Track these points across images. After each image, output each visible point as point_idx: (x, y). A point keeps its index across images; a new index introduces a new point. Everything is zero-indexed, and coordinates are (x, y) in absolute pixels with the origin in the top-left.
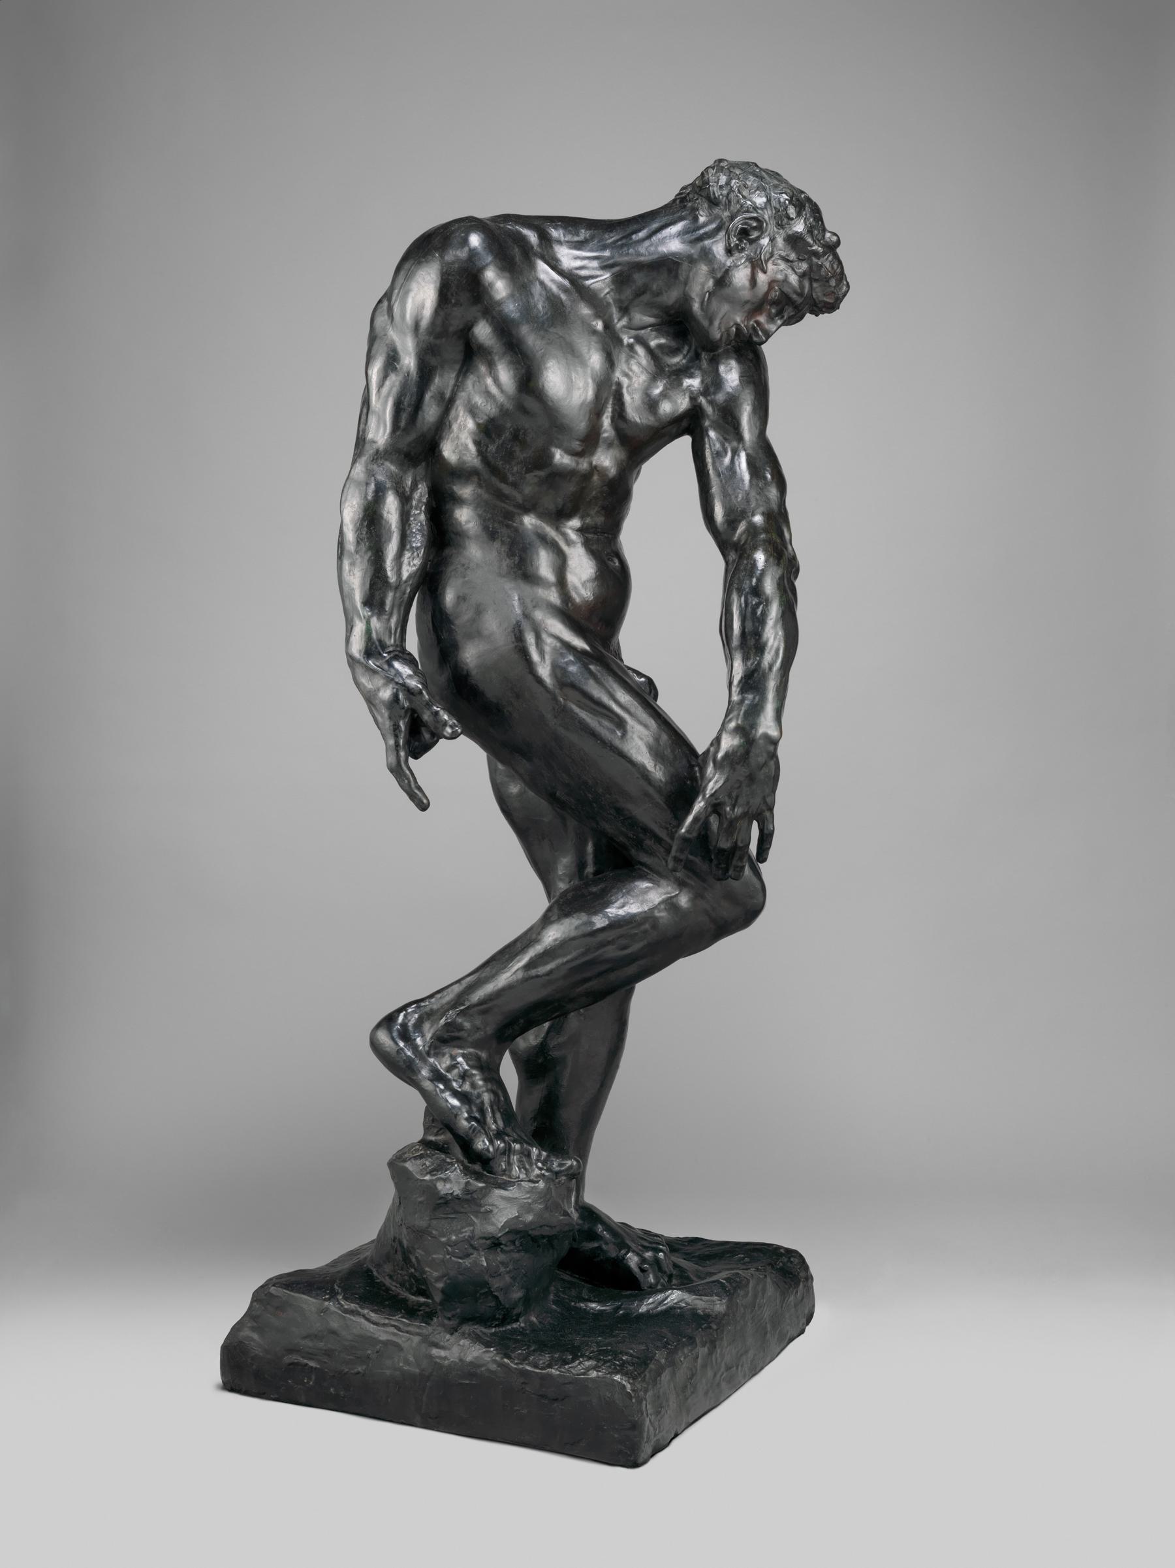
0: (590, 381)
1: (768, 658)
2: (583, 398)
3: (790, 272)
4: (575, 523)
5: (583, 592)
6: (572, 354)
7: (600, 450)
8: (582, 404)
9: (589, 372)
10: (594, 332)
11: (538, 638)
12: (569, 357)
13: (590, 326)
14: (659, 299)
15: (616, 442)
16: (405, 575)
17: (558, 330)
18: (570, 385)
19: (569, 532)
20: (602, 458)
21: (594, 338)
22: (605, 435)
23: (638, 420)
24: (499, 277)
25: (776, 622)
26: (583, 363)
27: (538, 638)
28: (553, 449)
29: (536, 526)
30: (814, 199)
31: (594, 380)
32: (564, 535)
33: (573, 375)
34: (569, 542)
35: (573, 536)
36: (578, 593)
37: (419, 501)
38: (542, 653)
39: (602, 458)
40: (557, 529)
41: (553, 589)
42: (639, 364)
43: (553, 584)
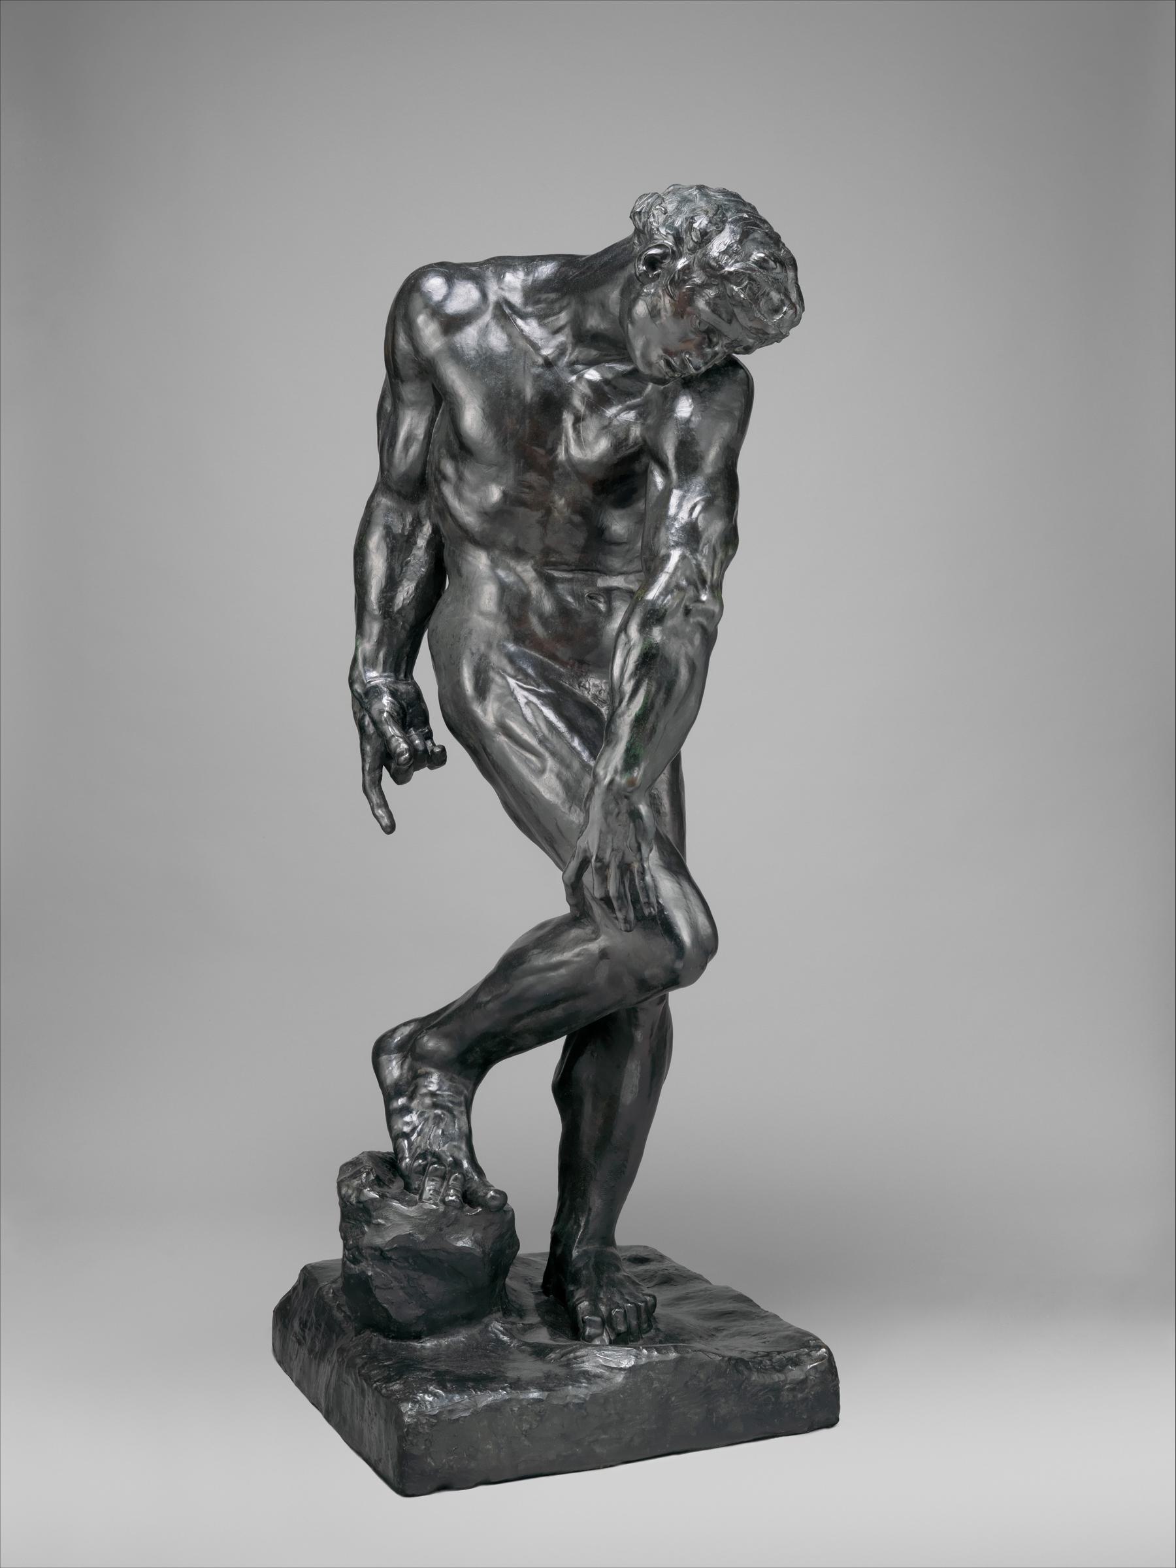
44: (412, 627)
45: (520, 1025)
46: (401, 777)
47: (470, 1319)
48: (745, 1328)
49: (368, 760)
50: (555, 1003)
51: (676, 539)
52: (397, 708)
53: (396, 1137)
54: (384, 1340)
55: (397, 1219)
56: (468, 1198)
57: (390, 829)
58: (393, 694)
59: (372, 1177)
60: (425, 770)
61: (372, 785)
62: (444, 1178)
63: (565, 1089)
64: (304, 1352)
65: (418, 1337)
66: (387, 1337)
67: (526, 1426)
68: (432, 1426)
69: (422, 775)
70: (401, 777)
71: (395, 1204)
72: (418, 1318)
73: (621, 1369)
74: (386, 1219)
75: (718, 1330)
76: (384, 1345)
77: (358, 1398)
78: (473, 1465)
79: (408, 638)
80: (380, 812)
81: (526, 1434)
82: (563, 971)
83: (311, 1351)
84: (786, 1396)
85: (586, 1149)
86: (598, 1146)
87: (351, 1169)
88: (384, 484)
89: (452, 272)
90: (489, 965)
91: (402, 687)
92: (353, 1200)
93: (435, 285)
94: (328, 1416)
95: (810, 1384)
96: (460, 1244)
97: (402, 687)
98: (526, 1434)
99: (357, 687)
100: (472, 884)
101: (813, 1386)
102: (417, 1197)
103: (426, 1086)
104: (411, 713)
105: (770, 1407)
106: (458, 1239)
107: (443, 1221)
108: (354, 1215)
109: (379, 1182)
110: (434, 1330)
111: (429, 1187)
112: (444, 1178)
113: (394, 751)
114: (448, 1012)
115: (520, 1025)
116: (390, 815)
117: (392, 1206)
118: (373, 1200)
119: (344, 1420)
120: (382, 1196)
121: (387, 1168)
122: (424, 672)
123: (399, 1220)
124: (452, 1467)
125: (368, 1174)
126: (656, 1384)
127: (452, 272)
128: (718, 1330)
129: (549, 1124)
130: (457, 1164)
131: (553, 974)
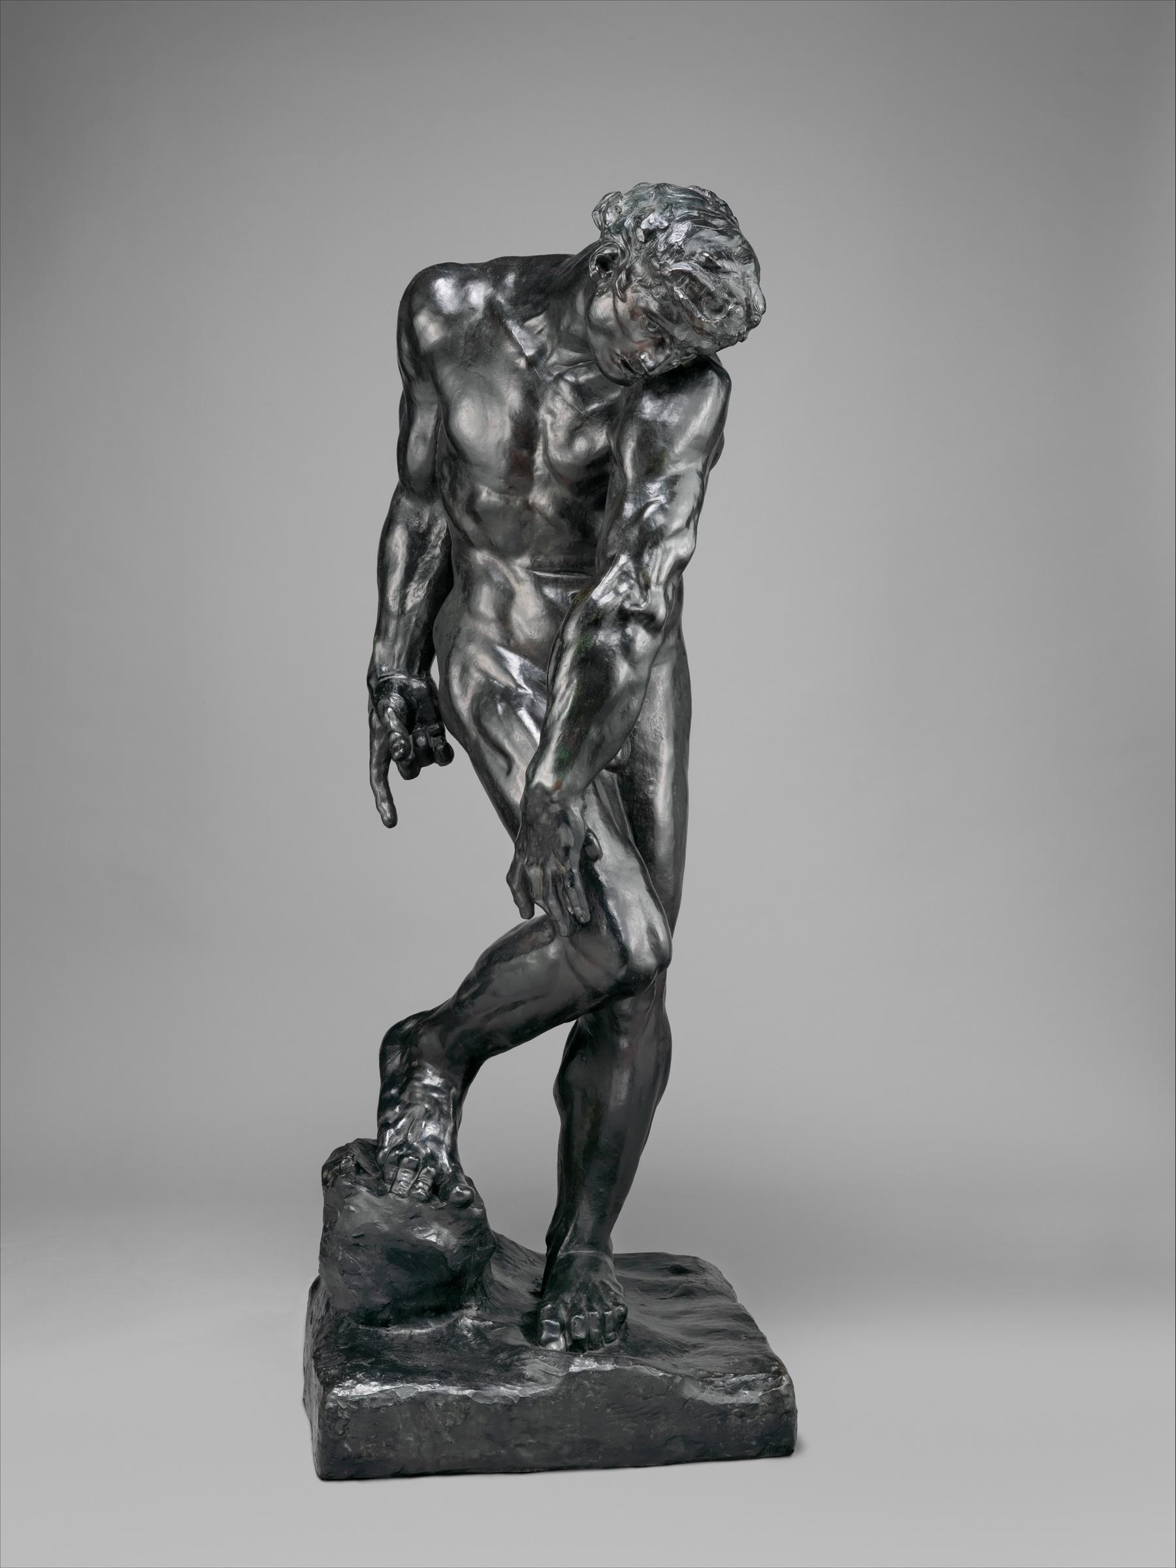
0: (507, 419)
1: (558, 707)
2: (500, 435)
3: (650, 299)
4: (525, 560)
5: (526, 630)
6: (490, 392)
7: (536, 488)
8: (499, 443)
9: (506, 409)
10: (516, 370)
11: (465, 670)
12: (487, 396)
13: (513, 363)
14: (668, 325)
15: (553, 480)
16: (409, 604)
17: (478, 370)
18: (485, 424)
19: (518, 569)
20: (538, 497)
21: (515, 376)
22: (538, 473)
23: (559, 458)
24: (431, 320)
25: (570, 672)
26: (501, 401)
27: (465, 670)
28: (481, 487)
29: (487, 563)
30: (736, 213)
31: (512, 418)
32: (514, 572)
33: (489, 413)
34: (519, 580)
35: (522, 574)
36: (522, 631)
37: (438, 536)
38: (464, 685)
39: (538, 497)
40: (508, 566)
41: (493, 625)
42: (564, 400)
43: (492, 620)
44: (425, 625)
46: (410, 772)
47: (439, 1312)
48: (721, 1348)
49: (375, 754)
50: (515, 1005)
53: (384, 1126)
56: (437, 1189)
57: (392, 823)
58: (403, 690)
60: (434, 766)
62: (416, 1170)
63: (564, 1090)
65: (385, 1324)
67: (449, 1422)
68: (353, 1412)
69: (430, 772)
72: (384, 1306)
74: (356, 1206)
75: (695, 1346)
78: (392, 1455)
79: (423, 634)
81: (450, 1430)
84: (734, 1421)
85: (577, 1153)
86: (598, 1152)
88: (406, 485)
89: (465, 274)
90: (466, 966)
91: (416, 684)
93: (444, 288)
95: (760, 1410)
97: (416, 684)
98: (450, 1430)
99: (373, 683)
100: (441, 884)
101: (765, 1413)
103: (420, 1080)
110: (402, 1318)
112: (416, 1170)
121: (370, 1148)
124: (370, 1455)
127: (465, 274)
128: (695, 1346)
129: (549, 1122)
130: (432, 1158)
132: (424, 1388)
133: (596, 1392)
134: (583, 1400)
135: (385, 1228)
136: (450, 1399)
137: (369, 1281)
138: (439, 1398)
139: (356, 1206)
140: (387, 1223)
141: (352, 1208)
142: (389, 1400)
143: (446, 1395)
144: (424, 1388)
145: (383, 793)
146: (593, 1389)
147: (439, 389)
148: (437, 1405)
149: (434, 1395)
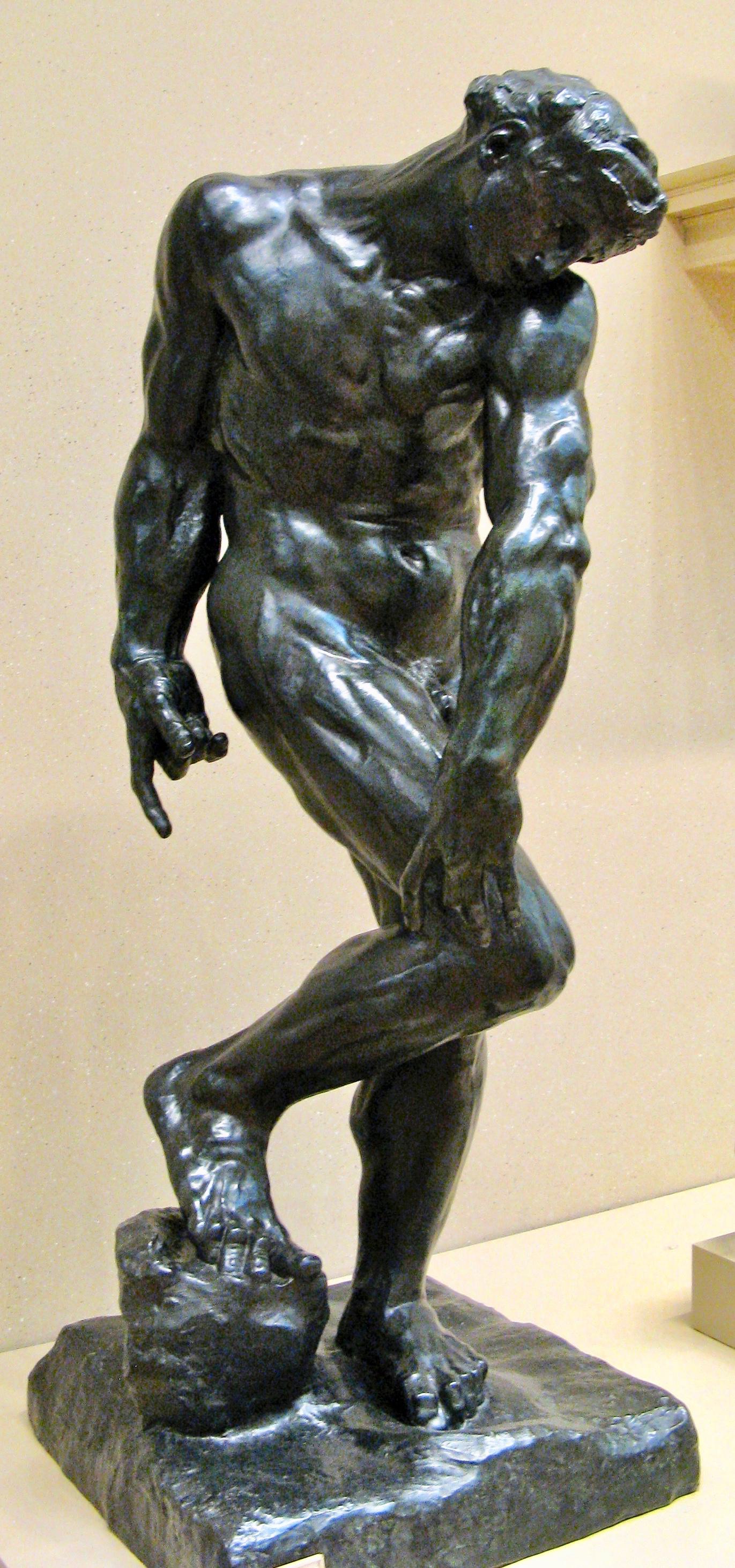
45: (333, 1060)
46: (175, 772)
51: (532, 469)
52: (172, 689)
54: (178, 1437)
55: (190, 1296)
57: (165, 832)
59: (159, 1246)
61: (142, 784)
64: (72, 1435)
66: (184, 1433)
67: (372, 1548)
70: (175, 772)
71: (189, 1277)
72: (221, 1409)
73: (472, 1463)
74: (180, 1297)
76: (180, 1443)
77: (156, 1516)
80: (154, 812)
82: (391, 996)
83: (83, 1435)
87: (130, 1232)
92: (139, 1274)
94: (114, 1524)
96: (270, 1322)
100: (269, 895)
102: (214, 1267)
104: (187, 696)
105: (634, 1483)
106: (268, 1317)
107: (248, 1297)
108: (142, 1291)
109: (168, 1251)
110: (240, 1420)
111: (231, 1255)
113: (162, 743)
114: (235, 1045)
115: (333, 1060)
116: (164, 815)
117: (184, 1281)
118: (164, 1274)
119: (137, 1534)
120: (175, 1269)
121: (176, 1227)
122: (200, 650)
123: (196, 1294)
125: (154, 1243)
126: (513, 1477)
131: (381, 1000)
132: (339, 1512)
133: (519, 1473)
134: (506, 1486)
135: (222, 1318)
136: (369, 1520)
137: (200, 1383)
138: (357, 1521)
139: (180, 1297)
140: (224, 1312)
141: (174, 1300)
142: (301, 1538)
143: (359, 1516)
144: (339, 1512)
145: (150, 799)
146: (515, 1470)
147: (476, 198)
148: (356, 1531)
149: (350, 1519)
